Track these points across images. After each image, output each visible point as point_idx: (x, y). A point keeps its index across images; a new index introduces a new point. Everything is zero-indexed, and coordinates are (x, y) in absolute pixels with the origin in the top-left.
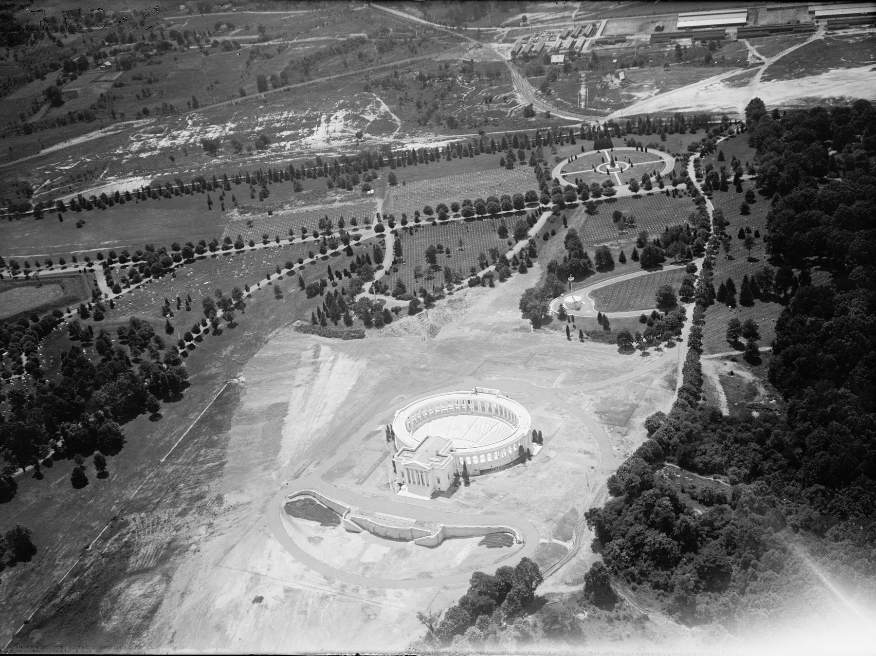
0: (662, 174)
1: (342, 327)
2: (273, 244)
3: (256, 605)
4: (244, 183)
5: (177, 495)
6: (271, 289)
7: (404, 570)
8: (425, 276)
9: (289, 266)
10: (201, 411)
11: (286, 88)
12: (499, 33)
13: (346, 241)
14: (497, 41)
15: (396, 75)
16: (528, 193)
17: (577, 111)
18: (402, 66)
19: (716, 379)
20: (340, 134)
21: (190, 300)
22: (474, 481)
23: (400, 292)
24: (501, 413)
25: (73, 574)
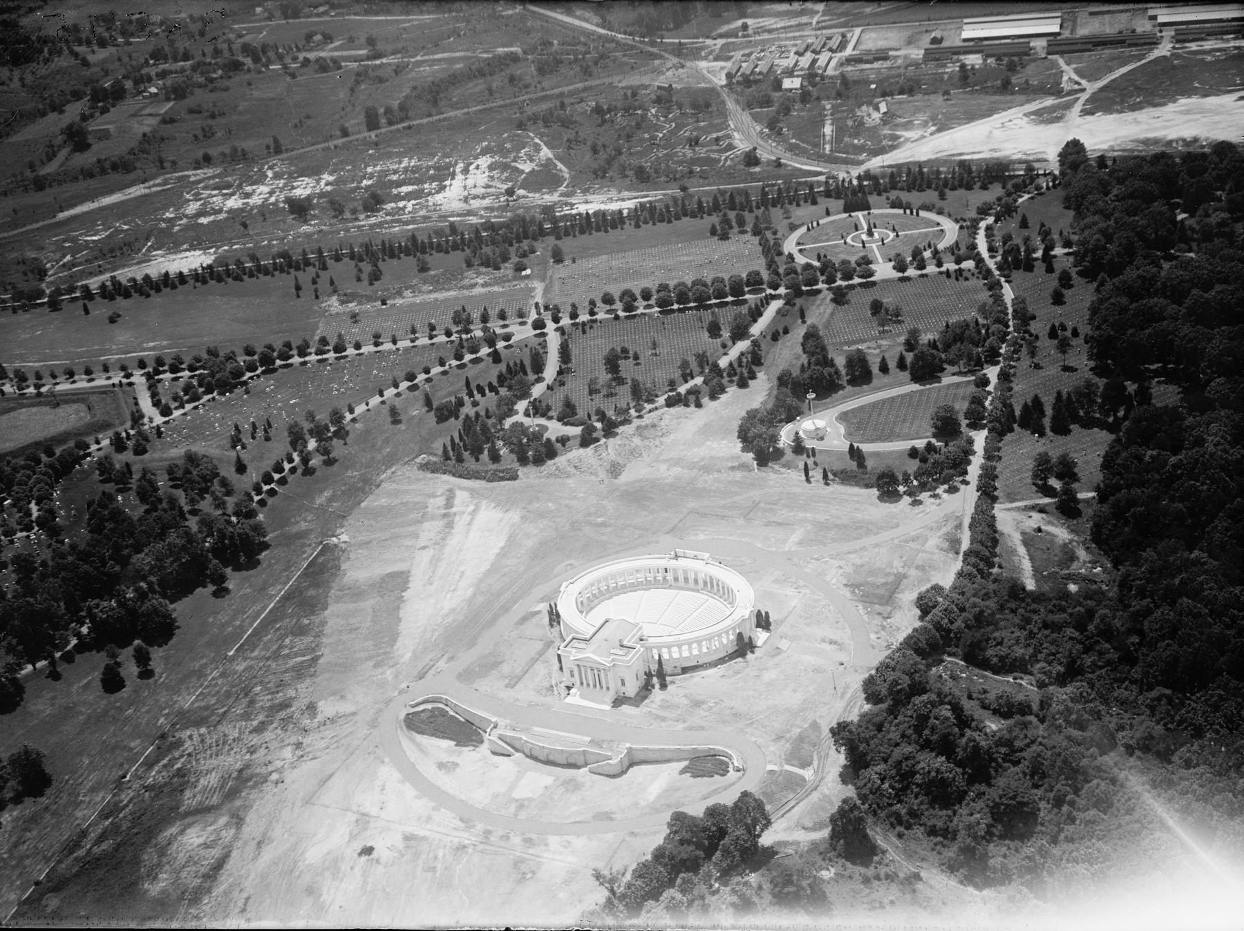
0: (940, 247)
1: (485, 464)
2: (388, 346)
3: (364, 858)
4: (346, 260)
5: (252, 702)
6: (385, 410)
7: (574, 809)
8: (604, 392)
9: (411, 377)
10: (285, 583)
11: (405, 124)
12: (708, 47)
13: (491, 342)
14: (705, 58)
15: (563, 106)
16: (749, 275)
17: (819, 157)
18: (571, 94)
19: (1016, 538)
20: (483, 190)
21: (270, 426)
22: (673, 682)
23: (568, 414)
24: (712, 586)
25: (104, 815)
